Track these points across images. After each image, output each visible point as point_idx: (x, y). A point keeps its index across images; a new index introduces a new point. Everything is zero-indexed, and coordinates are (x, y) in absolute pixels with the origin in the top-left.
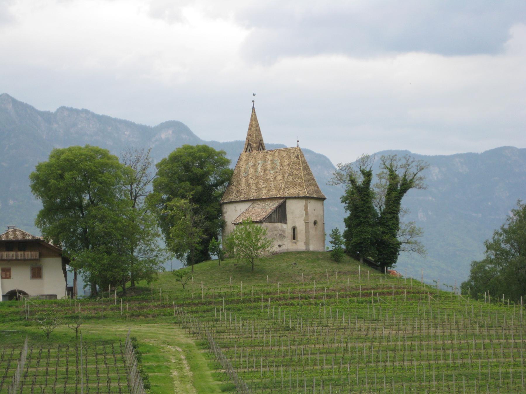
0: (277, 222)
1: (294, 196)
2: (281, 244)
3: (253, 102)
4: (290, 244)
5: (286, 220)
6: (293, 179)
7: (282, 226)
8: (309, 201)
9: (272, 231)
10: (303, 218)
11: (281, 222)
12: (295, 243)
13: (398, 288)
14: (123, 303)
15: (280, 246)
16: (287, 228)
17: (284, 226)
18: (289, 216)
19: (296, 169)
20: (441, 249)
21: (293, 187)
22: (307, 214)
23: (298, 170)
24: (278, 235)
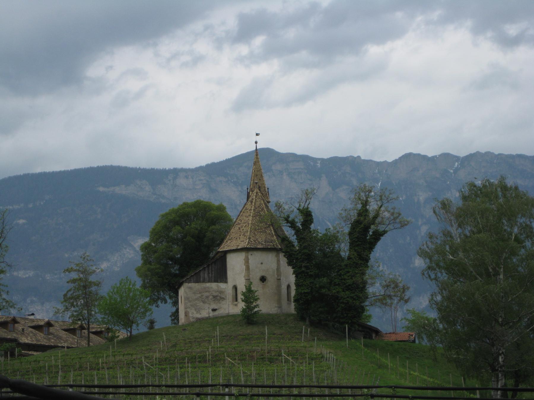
0: (209, 282)
1: (232, 248)
2: (216, 307)
3: (256, 143)
4: (231, 306)
5: (226, 278)
6: (239, 228)
7: (218, 286)
8: (250, 253)
9: (200, 293)
10: (243, 274)
11: (216, 281)
12: (236, 305)
13: (55, 377)
14: (531, 330)
15: (214, 310)
16: (226, 288)
17: (222, 285)
18: (229, 273)
19: (246, 216)
20: (404, 289)
21: (237, 238)
22: (248, 268)
23: (247, 217)
24: (211, 297)
